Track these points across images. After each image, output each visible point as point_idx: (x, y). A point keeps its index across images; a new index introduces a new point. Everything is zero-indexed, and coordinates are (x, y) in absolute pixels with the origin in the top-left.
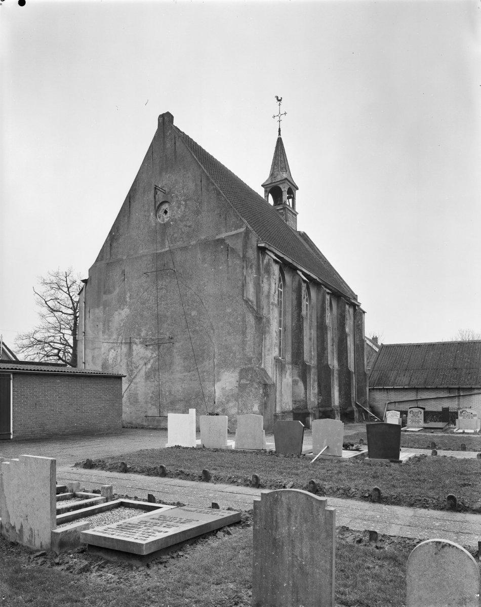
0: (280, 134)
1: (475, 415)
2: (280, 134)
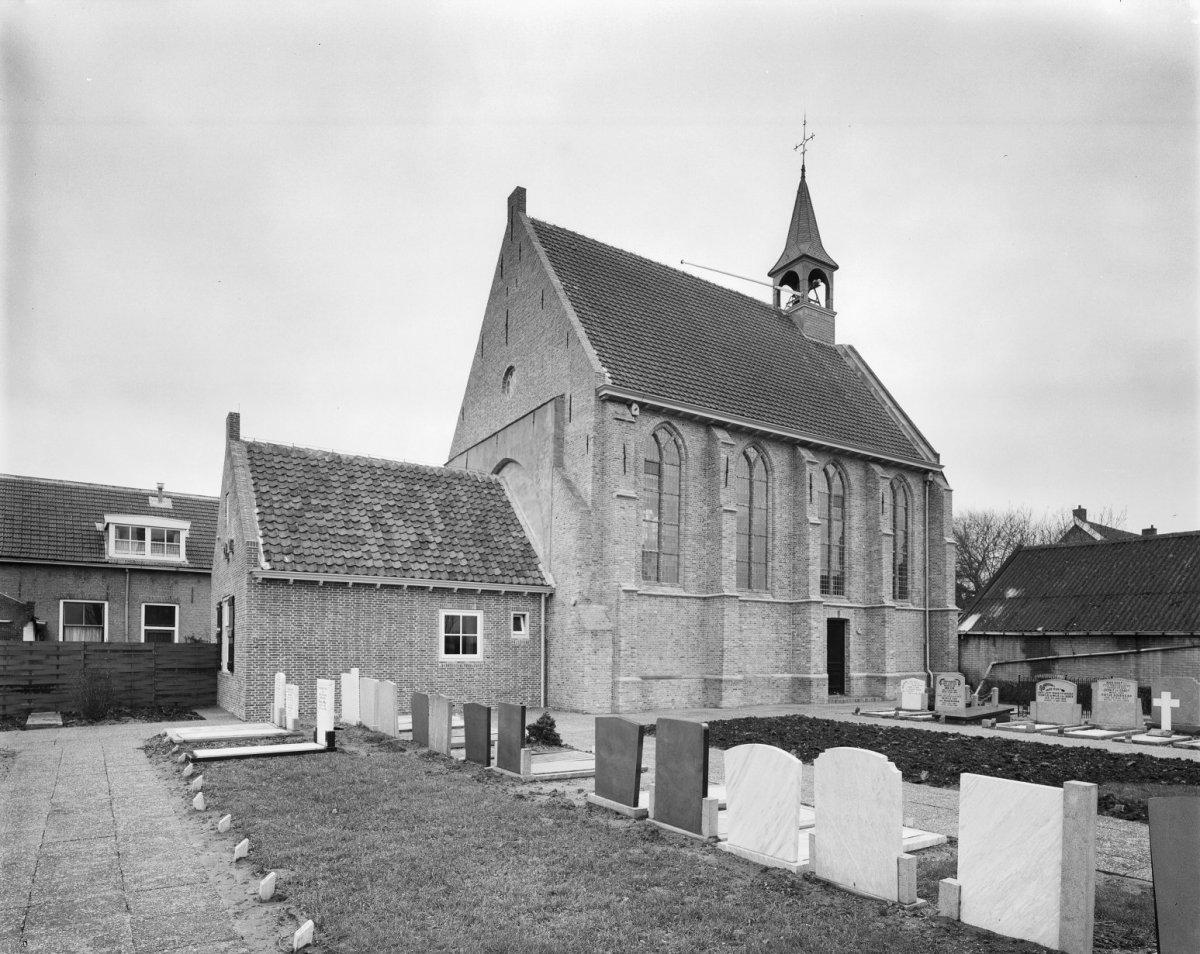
0: (803, 177)
1: (1070, 695)
2: (803, 177)
